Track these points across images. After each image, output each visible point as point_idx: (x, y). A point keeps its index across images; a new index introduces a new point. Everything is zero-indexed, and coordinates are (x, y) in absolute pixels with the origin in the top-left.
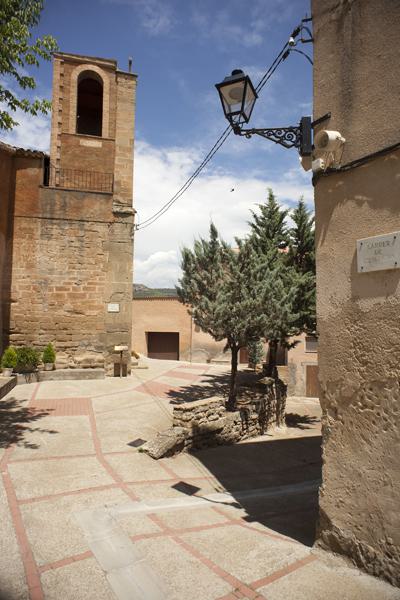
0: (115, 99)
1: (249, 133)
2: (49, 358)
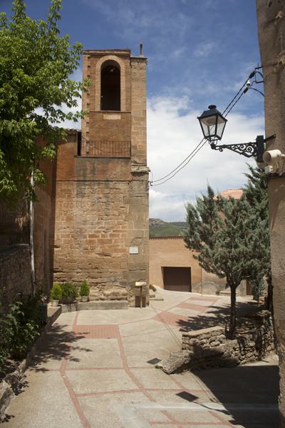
0: (129, 80)
1: (222, 147)
2: (85, 292)
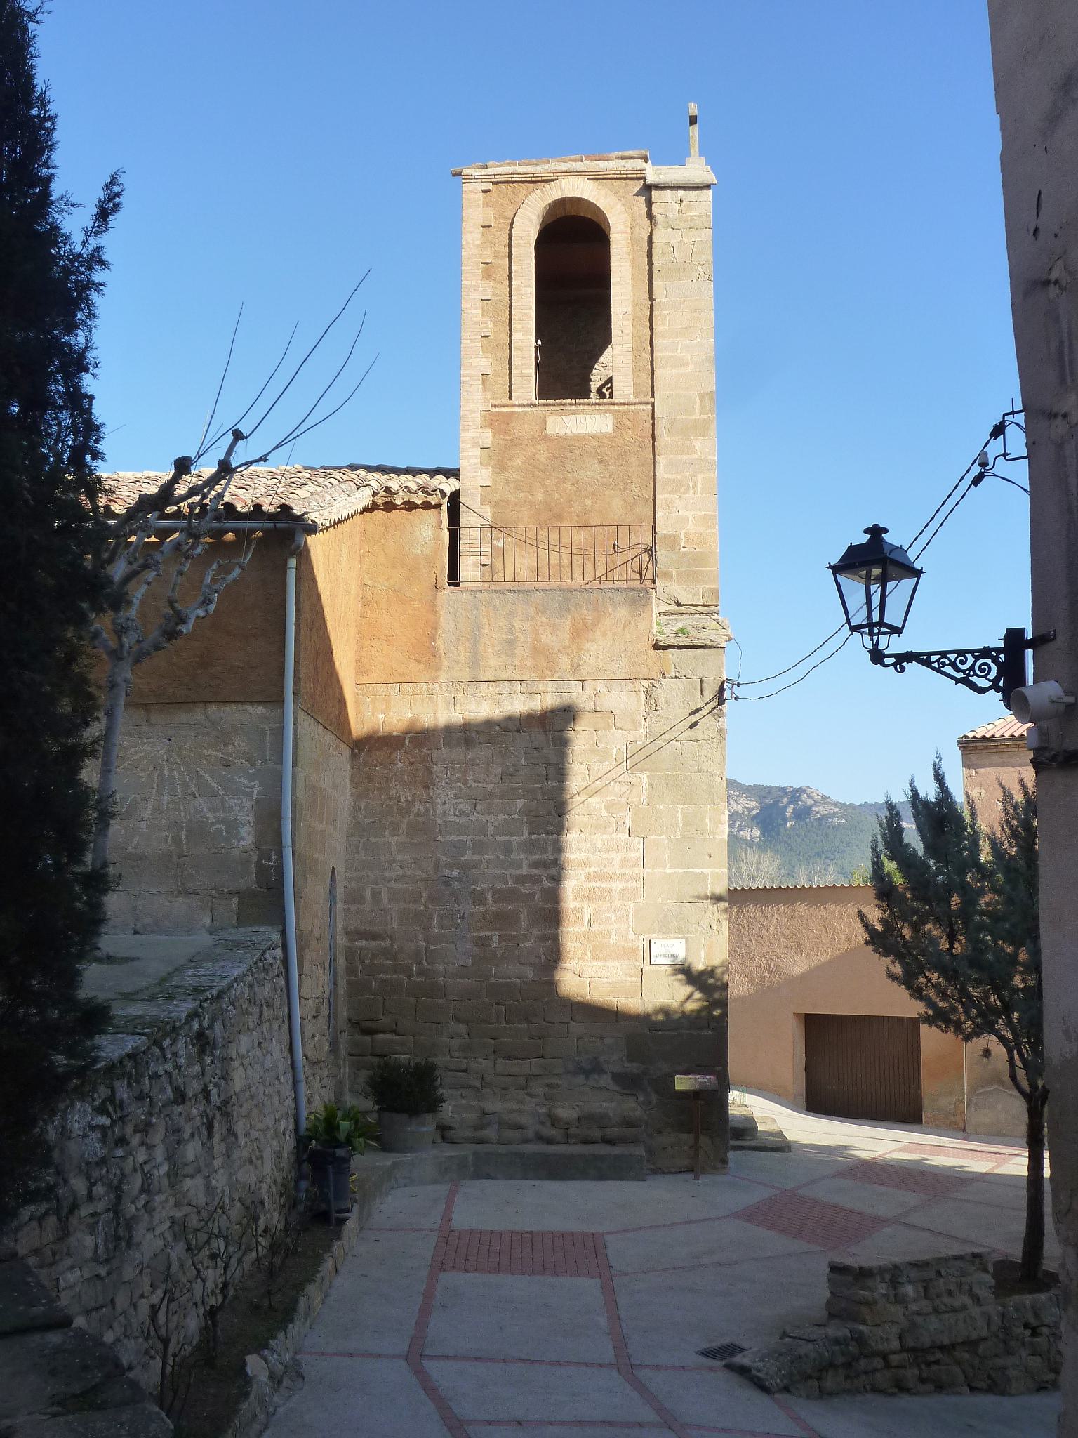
1: (902, 659)
